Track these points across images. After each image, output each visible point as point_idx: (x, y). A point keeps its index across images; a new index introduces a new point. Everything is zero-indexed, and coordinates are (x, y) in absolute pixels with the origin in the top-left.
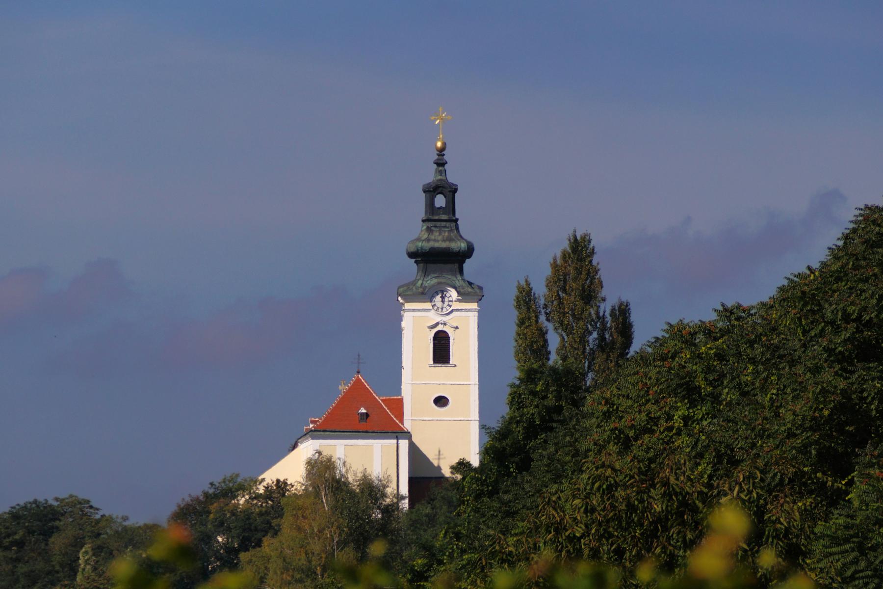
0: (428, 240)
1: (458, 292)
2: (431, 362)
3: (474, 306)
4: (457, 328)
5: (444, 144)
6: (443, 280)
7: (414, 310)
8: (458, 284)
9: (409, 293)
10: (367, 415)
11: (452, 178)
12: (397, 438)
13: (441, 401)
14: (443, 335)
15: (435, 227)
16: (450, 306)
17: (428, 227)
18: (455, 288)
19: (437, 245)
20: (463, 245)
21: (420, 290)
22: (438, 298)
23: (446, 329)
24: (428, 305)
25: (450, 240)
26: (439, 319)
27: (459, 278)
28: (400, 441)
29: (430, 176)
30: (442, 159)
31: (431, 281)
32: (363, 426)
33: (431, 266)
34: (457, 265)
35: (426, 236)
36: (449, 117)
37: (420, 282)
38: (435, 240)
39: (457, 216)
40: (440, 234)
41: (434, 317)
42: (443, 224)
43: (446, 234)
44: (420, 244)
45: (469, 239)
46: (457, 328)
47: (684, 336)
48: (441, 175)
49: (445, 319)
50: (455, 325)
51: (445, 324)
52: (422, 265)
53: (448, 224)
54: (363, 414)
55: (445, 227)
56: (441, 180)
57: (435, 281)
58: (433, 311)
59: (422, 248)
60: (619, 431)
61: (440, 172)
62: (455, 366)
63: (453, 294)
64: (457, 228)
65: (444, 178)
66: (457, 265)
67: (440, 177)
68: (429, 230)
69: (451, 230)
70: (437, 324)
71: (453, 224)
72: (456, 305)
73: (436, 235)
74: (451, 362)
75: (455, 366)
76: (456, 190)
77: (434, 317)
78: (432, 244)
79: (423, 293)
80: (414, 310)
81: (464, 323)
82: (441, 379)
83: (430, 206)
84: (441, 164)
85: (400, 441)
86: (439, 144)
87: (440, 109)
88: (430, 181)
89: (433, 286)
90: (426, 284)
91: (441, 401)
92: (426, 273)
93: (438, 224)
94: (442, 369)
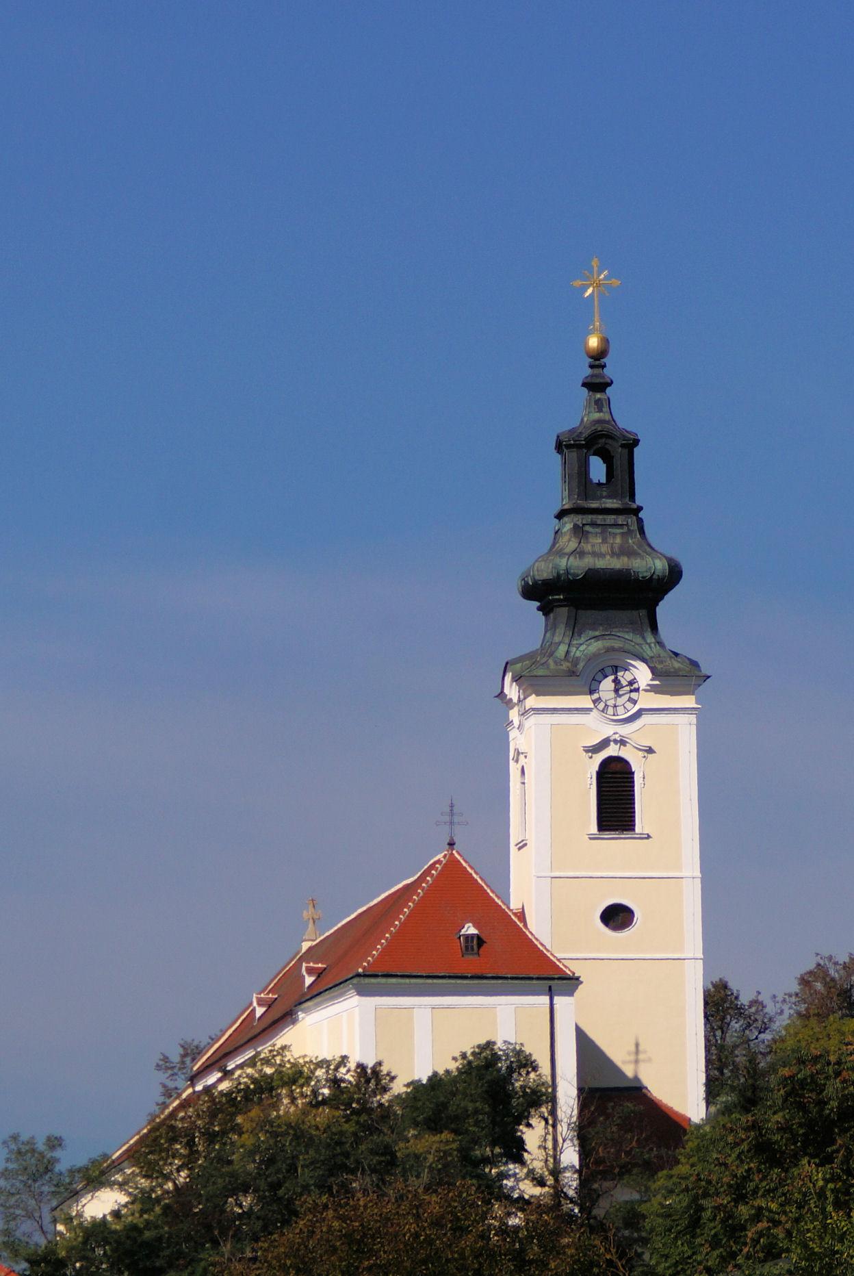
0: (580, 553)
1: (653, 670)
2: (594, 828)
3: (689, 701)
4: (650, 751)
5: (605, 342)
6: (617, 644)
7: (554, 711)
8: (648, 653)
9: (541, 672)
10: (480, 941)
11: (626, 418)
12: (551, 993)
13: (617, 916)
14: (619, 767)
15: (593, 524)
16: (635, 702)
17: (576, 527)
18: (644, 660)
19: (601, 564)
20: (660, 566)
21: (565, 666)
22: (607, 684)
23: (625, 753)
24: (585, 701)
25: (630, 553)
26: (608, 730)
27: (650, 638)
28: (558, 1000)
29: (575, 413)
30: (603, 376)
31: (588, 647)
32: (472, 963)
33: (587, 615)
34: (643, 613)
35: (573, 545)
36: (616, 282)
37: (562, 649)
38: (594, 554)
39: (640, 500)
40: (604, 541)
41: (597, 727)
42: (610, 519)
43: (618, 540)
44: (563, 563)
45: (669, 555)
46: (650, 751)
47: (415, 1085)
48: (600, 410)
49: (625, 730)
50: (647, 743)
51: (623, 742)
52: (563, 612)
53: (621, 519)
54: (472, 936)
55: (616, 525)
56: (599, 421)
57: (595, 646)
58: (595, 713)
59: (567, 572)
60: (363, 1252)
61: (599, 403)
62: (649, 837)
63: (642, 674)
64: (642, 531)
65: (607, 417)
66: (643, 613)
67: (597, 416)
68: (579, 531)
69: (630, 532)
70: (605, 743)
71: (632, 520)
72: (647, 700)
73: (595, 541)
74: (638, 829)
75: (649, 837)
76: (636, 442)
77: (597, 727)
78: (589, 562)
79: (572, 673)
80: (554, 711)
81: (668, 744)
82: (616, 866)
83: (580, 481)
84: (597, 386)
85: (557, 999)
86: (593, 342)
87: (595, 263)
88: (575, 423)
89: (595, 656)
90: (577, 653)
91: (617, 916)
92: (575, 628)
93: (599, 519)
94: (616, 846)
